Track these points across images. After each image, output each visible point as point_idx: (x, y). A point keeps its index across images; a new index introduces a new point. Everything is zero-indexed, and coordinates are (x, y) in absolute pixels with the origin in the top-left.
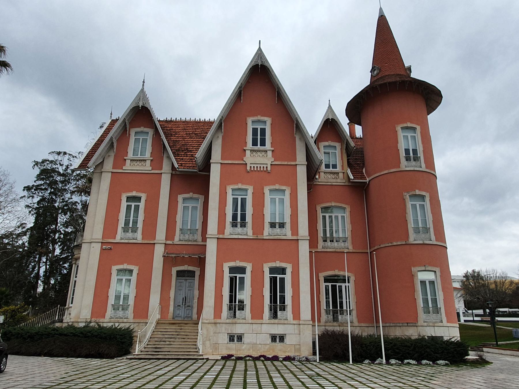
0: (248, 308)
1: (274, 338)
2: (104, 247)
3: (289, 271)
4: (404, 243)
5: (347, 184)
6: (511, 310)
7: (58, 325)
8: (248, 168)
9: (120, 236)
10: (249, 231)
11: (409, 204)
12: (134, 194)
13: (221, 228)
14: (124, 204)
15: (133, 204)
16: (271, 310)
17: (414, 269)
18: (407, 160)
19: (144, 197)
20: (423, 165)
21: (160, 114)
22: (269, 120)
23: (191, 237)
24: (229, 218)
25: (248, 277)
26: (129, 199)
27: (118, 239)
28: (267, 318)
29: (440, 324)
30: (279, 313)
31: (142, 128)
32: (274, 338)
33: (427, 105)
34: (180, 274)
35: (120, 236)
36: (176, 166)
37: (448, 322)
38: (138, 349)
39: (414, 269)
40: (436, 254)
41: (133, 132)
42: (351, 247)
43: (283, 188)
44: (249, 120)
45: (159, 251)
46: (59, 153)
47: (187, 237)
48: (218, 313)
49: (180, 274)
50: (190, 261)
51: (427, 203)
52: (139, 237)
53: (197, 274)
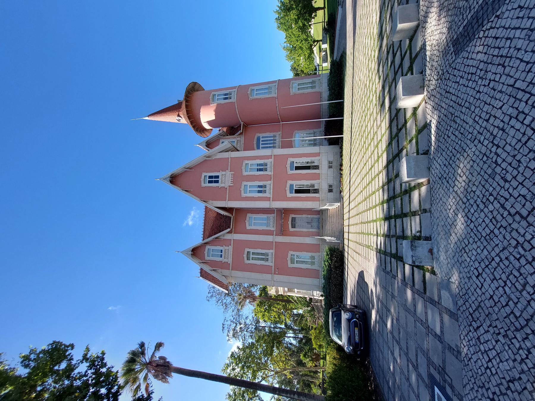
0: (313, 182)
7: (323, 303)
8: (232, 185)
9: (270, 263)
10: (269, 184)
12: (245, 256)
13: (268, 199)
15: (251, 256)
19: (247, 250)
21: (197, 239)
22: (204, 174)
23: (272, 220)
24: (260, 195)
26: (248, 259)
27: (272, 264)
30: (316, 164)
34: (293, 226)
35: (270, 263)
40: (283, 84)
41: (207, 258)
42: (279, 133)
43: (244, 164)
44: (203, 185)
46: (223, 328)
47: (271, 223)
48: (317, 199)
49: (293, 226)
50: (286, 219)
52: (271, 252)
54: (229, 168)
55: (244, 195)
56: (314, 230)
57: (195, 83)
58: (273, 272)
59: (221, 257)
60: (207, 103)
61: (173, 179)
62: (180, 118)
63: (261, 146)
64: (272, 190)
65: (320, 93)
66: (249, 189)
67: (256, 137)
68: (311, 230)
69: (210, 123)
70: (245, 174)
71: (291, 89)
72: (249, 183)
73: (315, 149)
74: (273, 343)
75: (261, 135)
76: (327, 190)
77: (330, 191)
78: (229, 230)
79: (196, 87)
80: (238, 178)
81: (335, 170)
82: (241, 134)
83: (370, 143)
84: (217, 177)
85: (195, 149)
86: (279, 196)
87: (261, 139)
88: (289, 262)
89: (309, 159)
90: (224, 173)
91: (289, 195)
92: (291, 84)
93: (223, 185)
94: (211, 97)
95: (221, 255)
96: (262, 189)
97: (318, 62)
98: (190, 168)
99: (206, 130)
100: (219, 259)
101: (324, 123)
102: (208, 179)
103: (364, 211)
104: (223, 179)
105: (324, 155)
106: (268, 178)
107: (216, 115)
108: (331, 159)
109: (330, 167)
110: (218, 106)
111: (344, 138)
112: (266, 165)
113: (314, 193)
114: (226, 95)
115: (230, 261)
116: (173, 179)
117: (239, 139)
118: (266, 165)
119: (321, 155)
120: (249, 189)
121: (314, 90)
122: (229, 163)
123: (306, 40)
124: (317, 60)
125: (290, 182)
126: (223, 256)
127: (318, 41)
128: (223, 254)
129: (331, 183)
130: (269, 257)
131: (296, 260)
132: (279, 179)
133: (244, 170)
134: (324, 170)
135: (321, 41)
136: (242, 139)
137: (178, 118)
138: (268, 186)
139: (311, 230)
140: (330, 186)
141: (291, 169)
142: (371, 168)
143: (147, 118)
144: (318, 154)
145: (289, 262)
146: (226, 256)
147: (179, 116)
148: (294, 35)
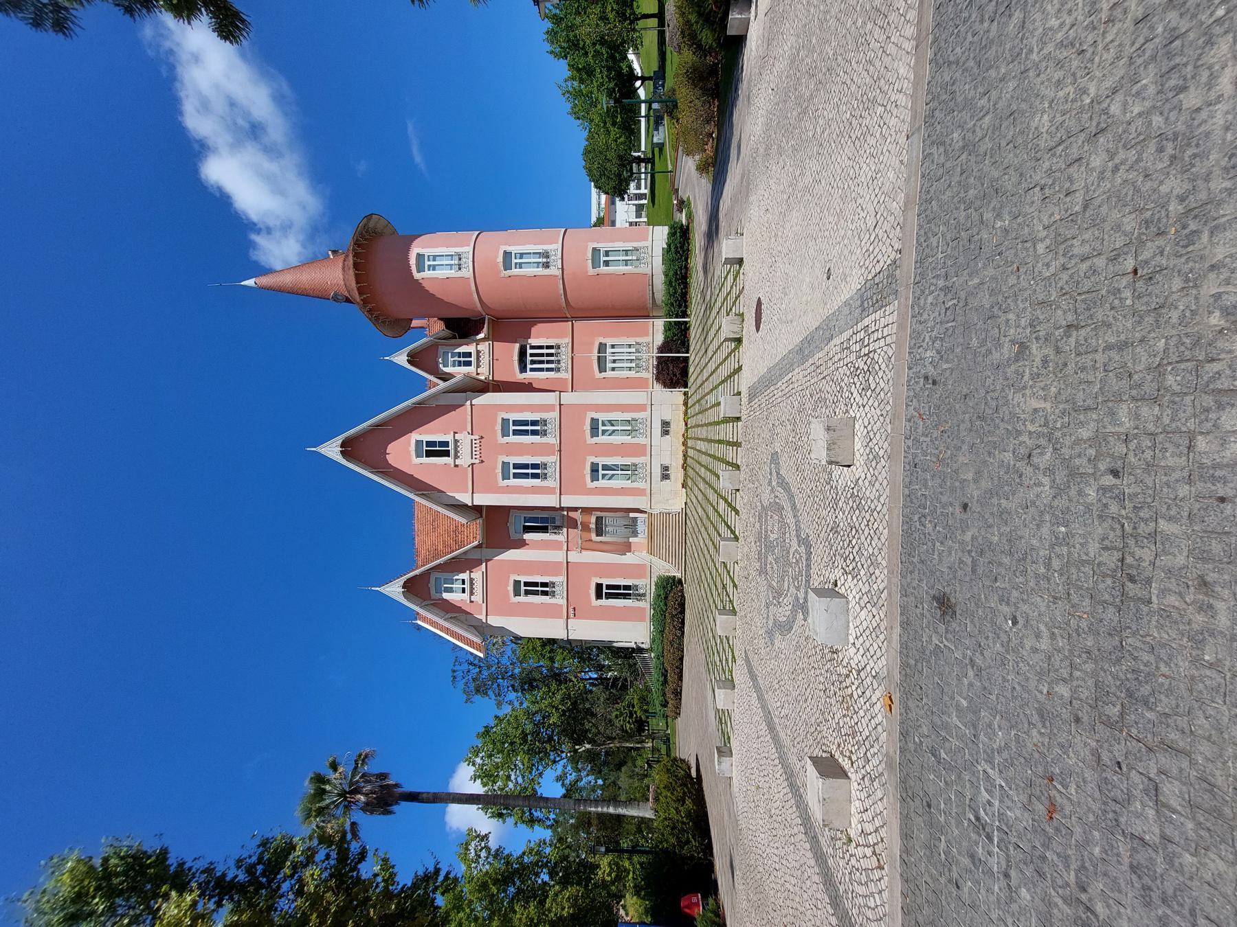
1: (666, 432)
6: (411, 496)
13: (549, 491)
32: (666, 432)
35: (560, 600)
36: (476, 543)
38: (678, 575)
53: (600, 514)
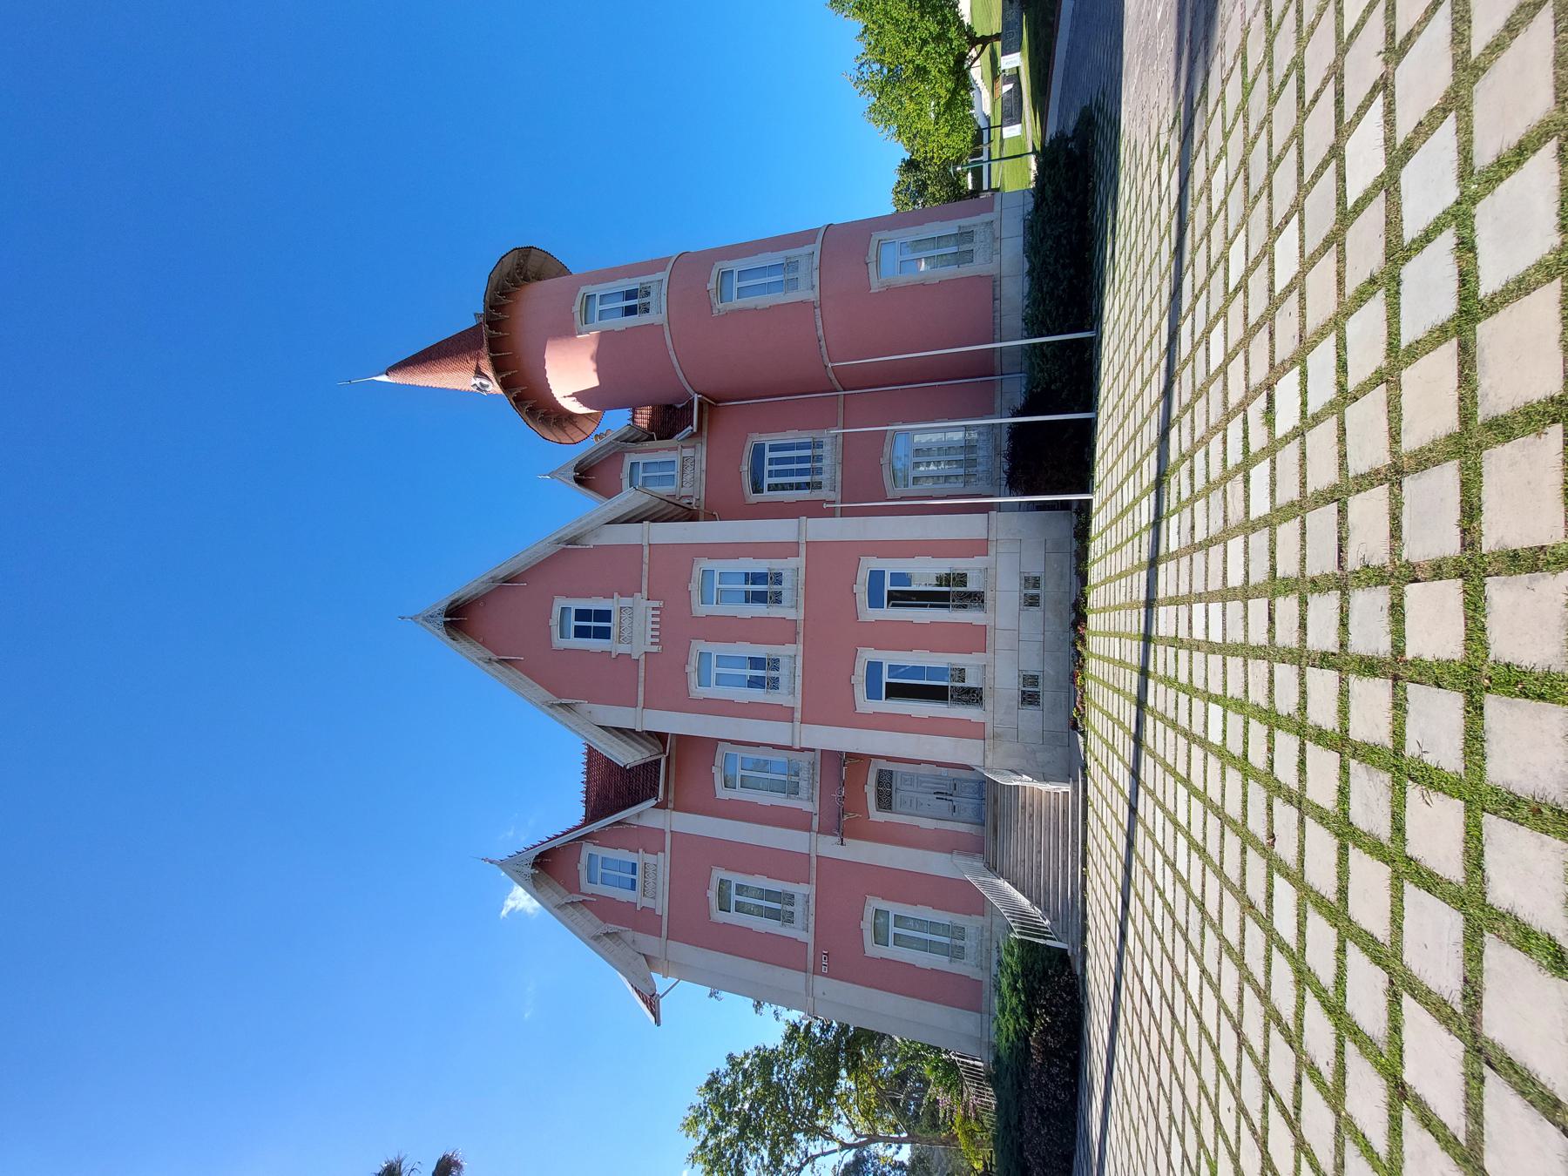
2: (824, 970)
3: (876, 564)
4: (818, 311)
5: (705, 440)
8: (655, 649)
9: (801, 932)
11: (737, 303)
12: (713, 895)
13: (785, 714)
14: (733, 918)
16: (965, 607)
17: (875, 287)
18: (647, 311)
20: (658, 276)
22: (560, 603)
23: (804, 774)
24: (758, 695)
25: (890, 566)
27: (808, 937)
28: (981, 615)
29: (996, 225)
30: (971, 587)
31: (580, 867)
33: (539, 277)
34: (885, 802)
35: (801, 932)
37: (992, 210)
39: (875, 287)
40: (845, 244)
44: (558, 643)
45: (829, 847)
48: (975, 731)
51: (737, 265)
52: (801, 890)
54: (645, 586)
55: (698, 692)
56: (962, 828)
57: (526, 252)
58: (811, 966)
59: (633, 888)
60: (566, 331)
61: (458, 618)
62: (485, 382)
63: (767, 481)
64: (799, 681)
65: (993, 282)
66: (716, 669)
67: (749, 447)
68: (948, 826)
69: (581, 397)
70: (700, 610)
71: (872, 267)
72: (716, 649)
73: (969, 527)
74: (835, 1062)
75: (768, 439)
76: (1016, 694)
77: (1029, 699)
78: (653, 802)
79: (533, 263)
80: (678, 628)
81: (1049, 615)
82: (692, 435)
83: (1145, 350)
84: (605, 615)
85: (529, 505)
86: (825, 703)
87: (768, 455)
88: (868, 936)
89: (945, 566)
90: (626, 601)
91: (865, 705)
92: (874, 244)
93: (623, 648)
94: (576, 308)
95: (633, 881)
96: (763, 673)
97: (987, 111)
98: (510, 579)
99: (571, 417)
100: (624, 895)
101: (1005, 429)
102: (574, 623)
103: (1120, 576)
104: (626, 624)
105: (1001, 545)
106: (784, 632)
107: (600, 372)
108: (1035, 569)
109: (1032, 601)
110: (605, 339)
111: (1095, 505)
112: (777, 578)
113: (959, 701)
114: (630, 295)
115: (661, 905)
116: (458, 618)
117: (688, 452)
118: (777, 578)
119: (992, 552)
120: (715, 670)
121: (966, 270)
122: (645, 567)
123: (940, 38)
124: (984, 102)
125: (868, 655)
126: (639, 885)
127: (985, 40)
128: (639, 877)
129: (1033, 667)
130: (798, 909)
131: (893, 930)
132: (827, 636)
133: (696, 598)
134: (1003, 611)
135: (997, 37)
136: (700, 454)
137: (478, 381)
138: (784, 662)
139: (948, 826)
140: (1032, 680)
141: (875, 602)
142: (1142, 426)
143: (384, 378)
144: (979, 547)
145: (868, 936)
146: (650, 886)
147: (479, 373)
148: (897, 23)
